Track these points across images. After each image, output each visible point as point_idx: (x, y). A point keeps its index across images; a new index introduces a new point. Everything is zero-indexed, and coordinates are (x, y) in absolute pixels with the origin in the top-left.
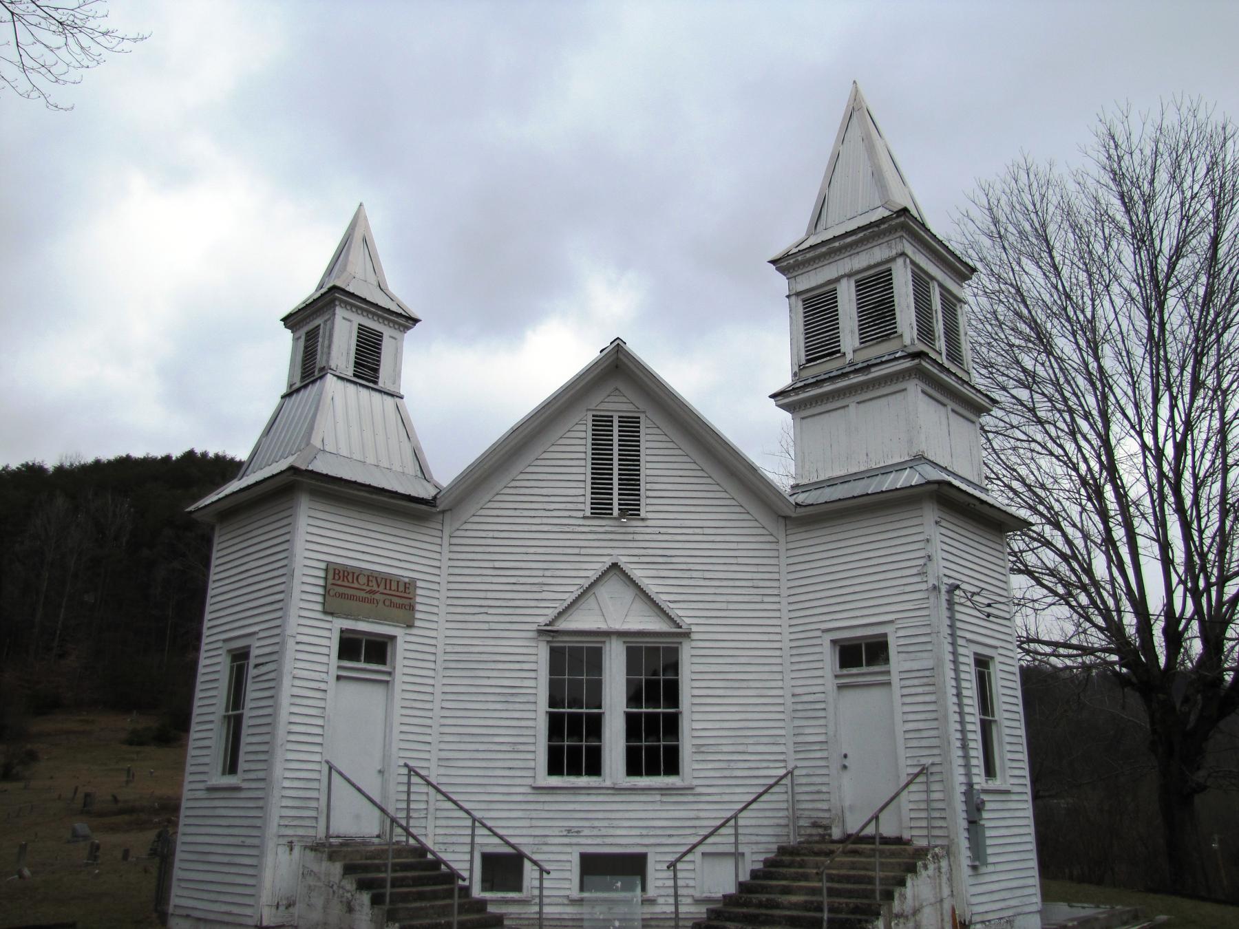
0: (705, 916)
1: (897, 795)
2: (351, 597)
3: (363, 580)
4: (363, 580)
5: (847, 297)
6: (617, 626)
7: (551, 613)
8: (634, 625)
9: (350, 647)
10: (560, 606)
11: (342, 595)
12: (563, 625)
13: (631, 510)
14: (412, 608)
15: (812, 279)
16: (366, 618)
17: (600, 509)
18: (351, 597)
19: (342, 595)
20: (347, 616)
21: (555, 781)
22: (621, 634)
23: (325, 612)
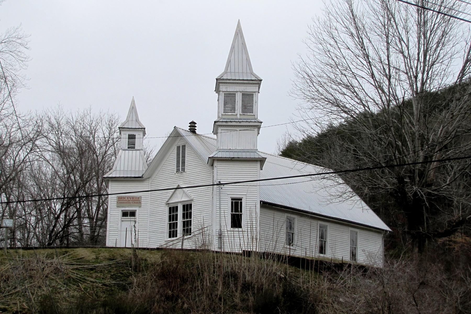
0: (376, 113)
1: (464, 2)
2: (123, 203)
3: (126, 198)
4: (126, 198)
5: (239, 98)
6: (180, 200)
7: (167, 200)
8: (184, 199)
9: (125, 214)
10: (168, 197)
11: (121, 203)
12: (170, 202)
13: (183, 170)
14: (140, 203)
15: (248, 116)
16: (128, 207)
17: (178, 170)
18: (123, 203)
19: (121, 203)
20: (123, 207)
21: (170, 239)
22: (180, 202)
23: (117, 207)
